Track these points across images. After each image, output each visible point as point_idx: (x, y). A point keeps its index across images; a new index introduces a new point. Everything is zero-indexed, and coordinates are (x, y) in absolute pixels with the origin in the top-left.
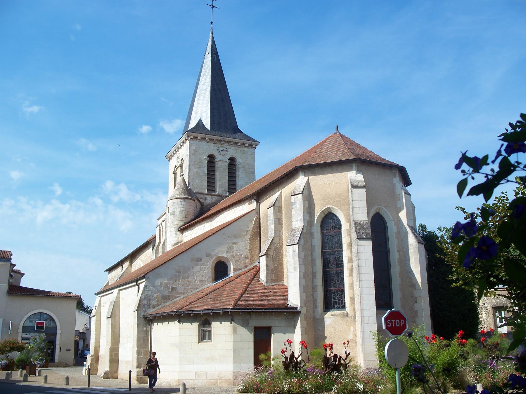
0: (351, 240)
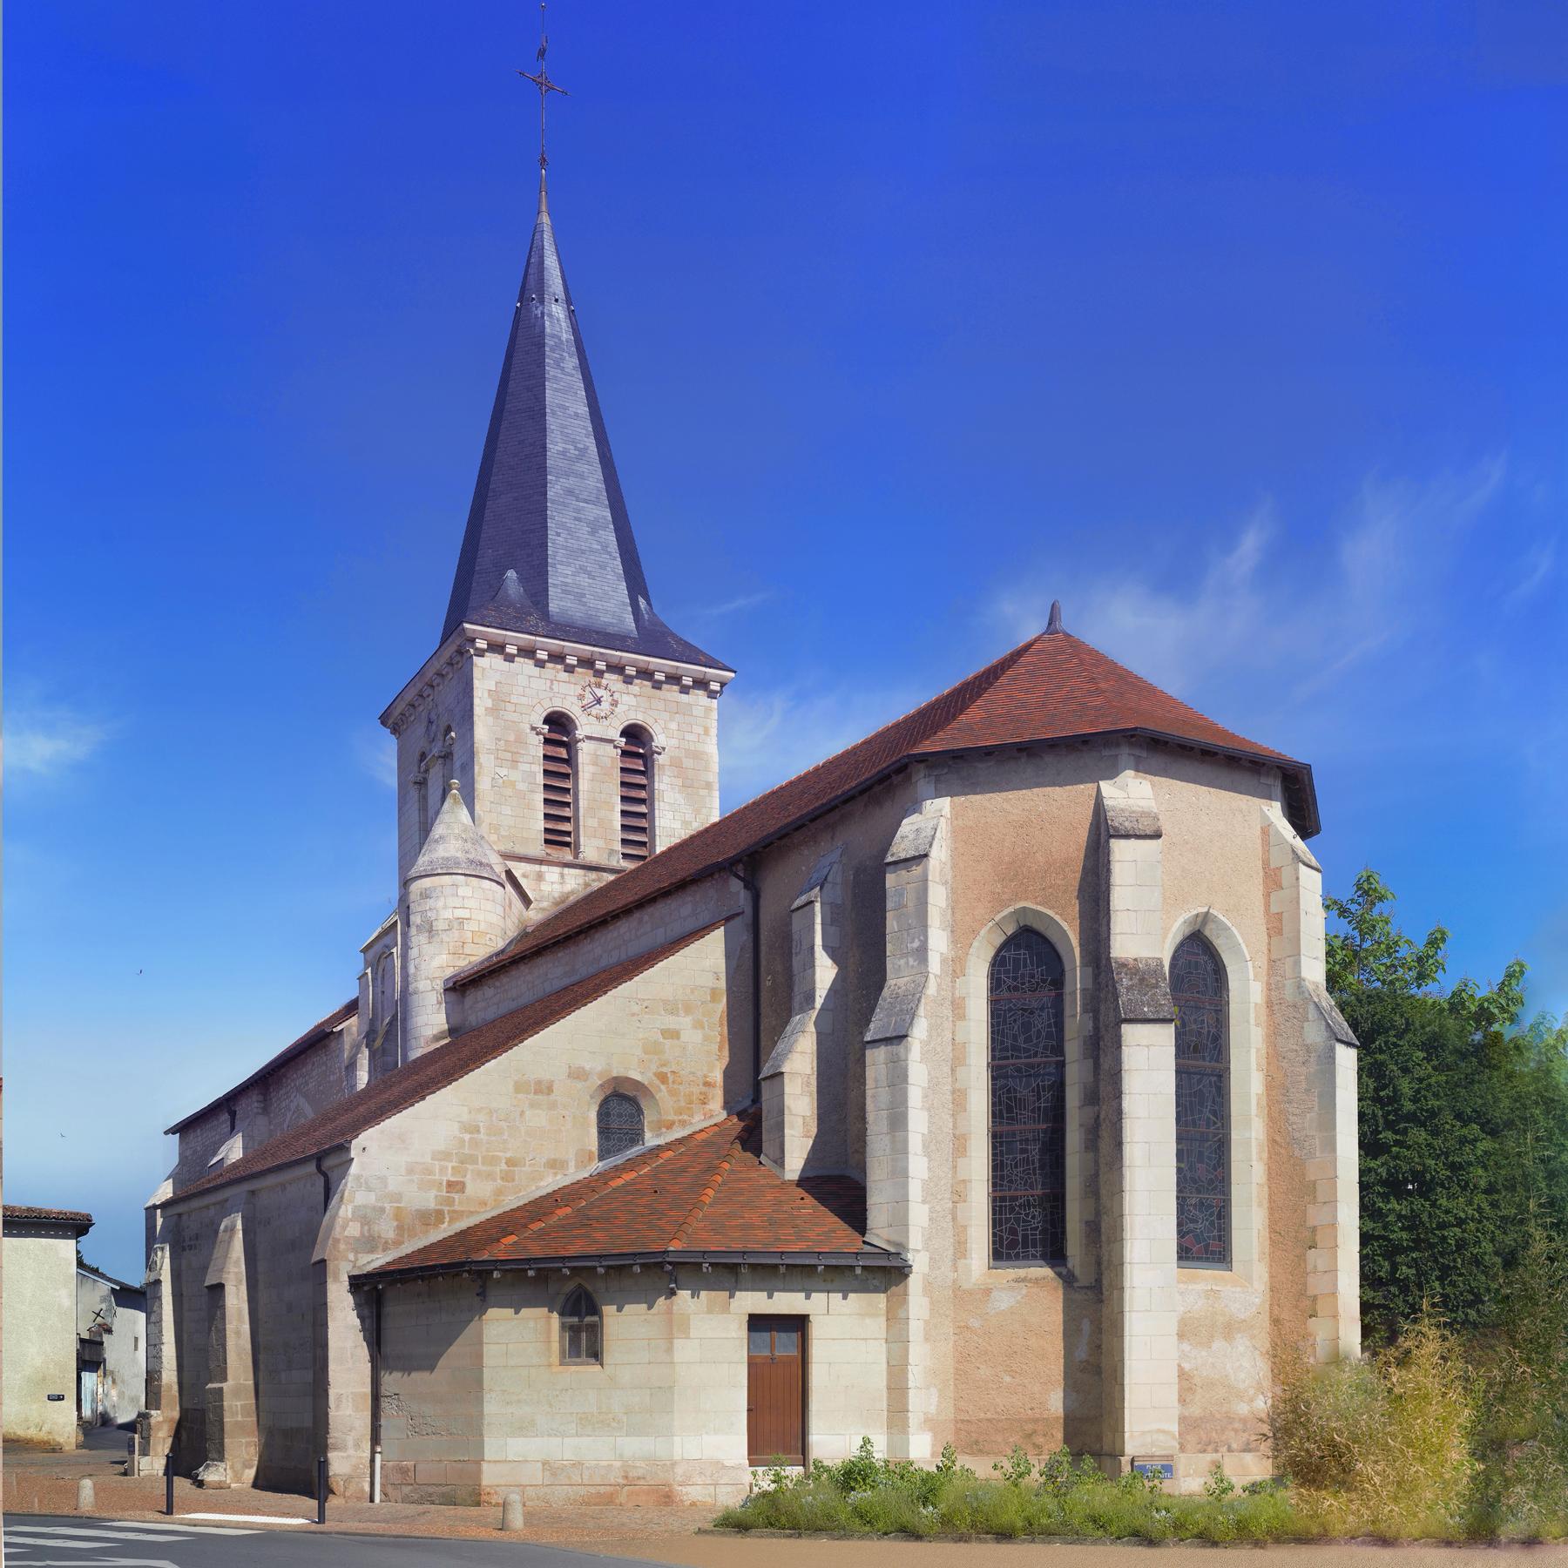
0: (1096, 1028)
